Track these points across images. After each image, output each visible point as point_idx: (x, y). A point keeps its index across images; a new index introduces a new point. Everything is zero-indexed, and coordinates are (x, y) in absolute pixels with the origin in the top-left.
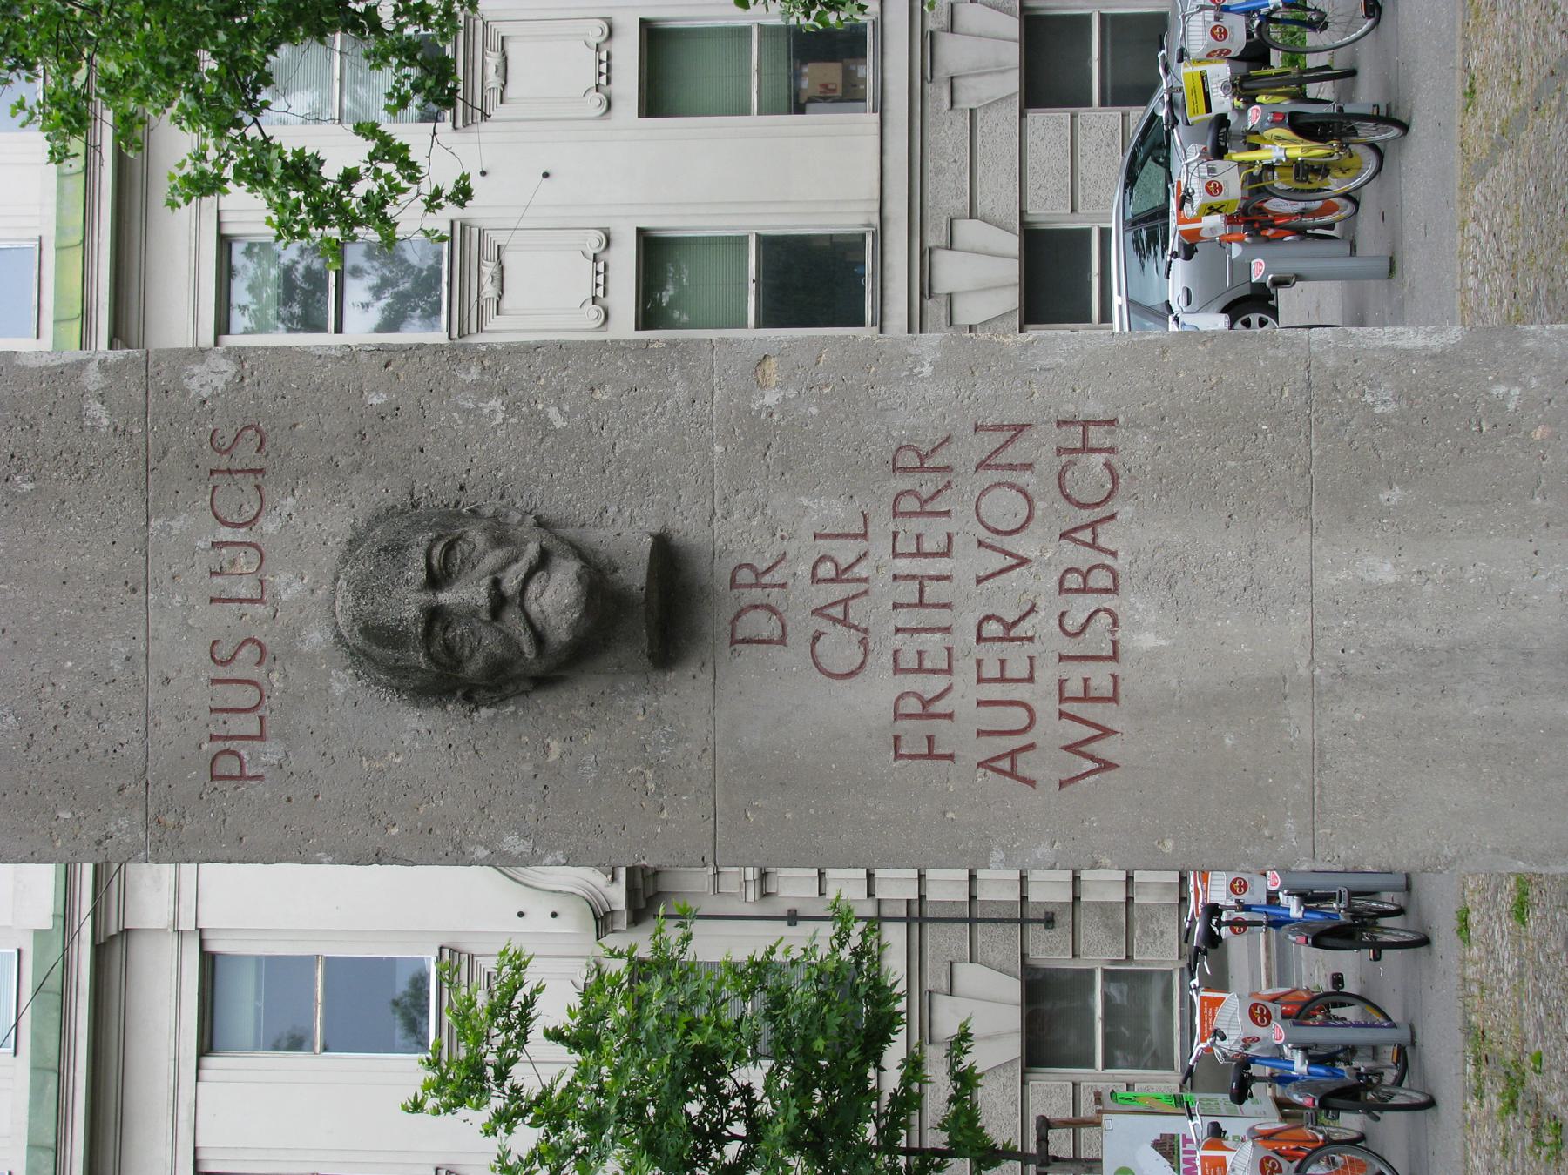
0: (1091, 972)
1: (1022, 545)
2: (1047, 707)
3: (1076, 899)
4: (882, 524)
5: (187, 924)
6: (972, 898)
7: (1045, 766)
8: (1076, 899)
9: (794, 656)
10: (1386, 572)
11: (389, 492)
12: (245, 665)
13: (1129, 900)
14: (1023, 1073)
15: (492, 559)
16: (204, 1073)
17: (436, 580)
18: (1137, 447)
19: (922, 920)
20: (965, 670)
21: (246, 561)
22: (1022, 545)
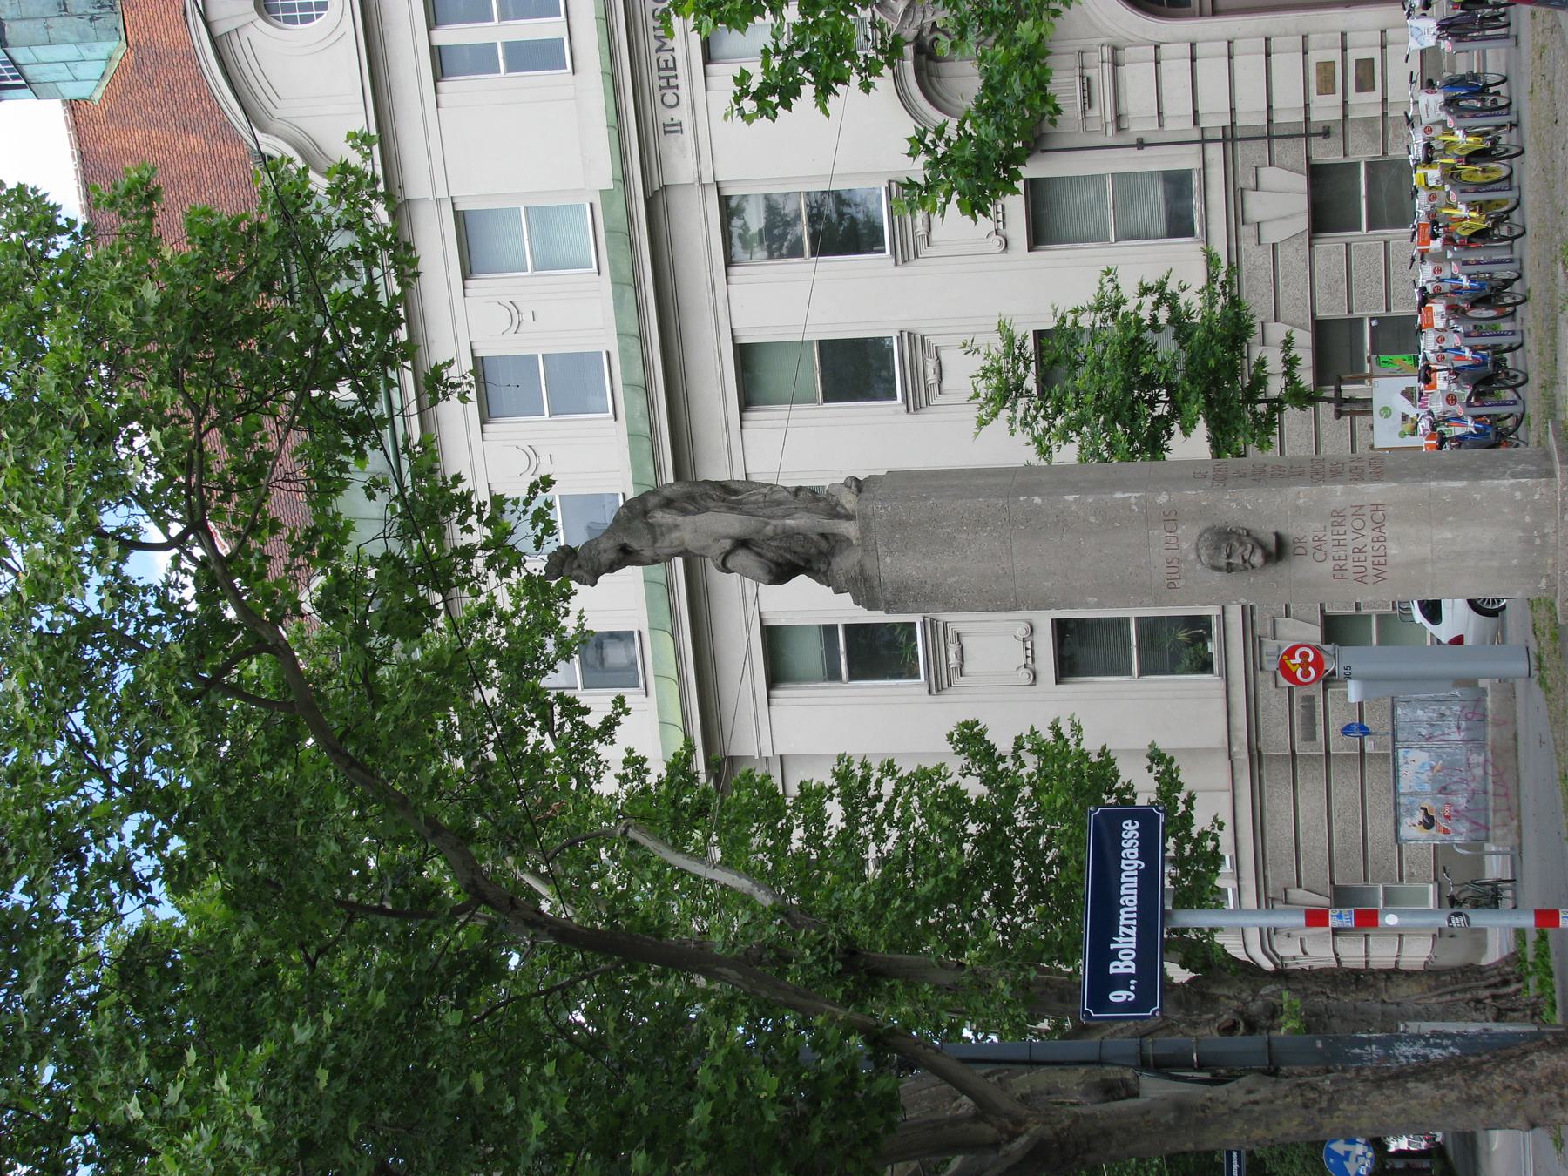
0: (1356, 165)
1: (1363, 532)
2: (1370, 567)
3: (1345, 116)
4: (1329, 528)
5: (708, 178)
6: (1270, 121)
7: (1369, 580)
8: (1345, 116)
9: (1309, 558)
10: (1449, 535)
11: (1209, 524)
12: (1175, 563)
13: (1384, 115)
14: (1311, 239)
15: (1241, 550)
16: (731, 278)
17: (1229, 556)
18: (1390, 510)
19: (1234, 139)
20: (1350, 562)
21: (1173, 540)
22: (1363, 532)
